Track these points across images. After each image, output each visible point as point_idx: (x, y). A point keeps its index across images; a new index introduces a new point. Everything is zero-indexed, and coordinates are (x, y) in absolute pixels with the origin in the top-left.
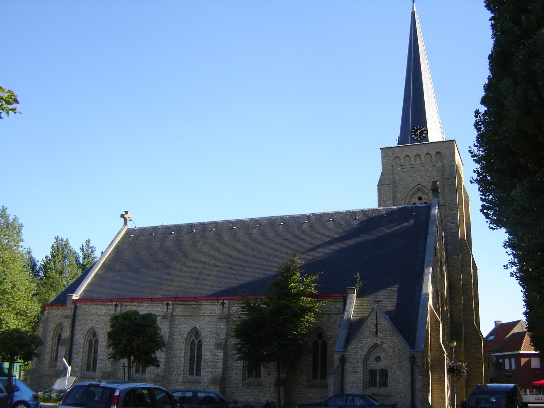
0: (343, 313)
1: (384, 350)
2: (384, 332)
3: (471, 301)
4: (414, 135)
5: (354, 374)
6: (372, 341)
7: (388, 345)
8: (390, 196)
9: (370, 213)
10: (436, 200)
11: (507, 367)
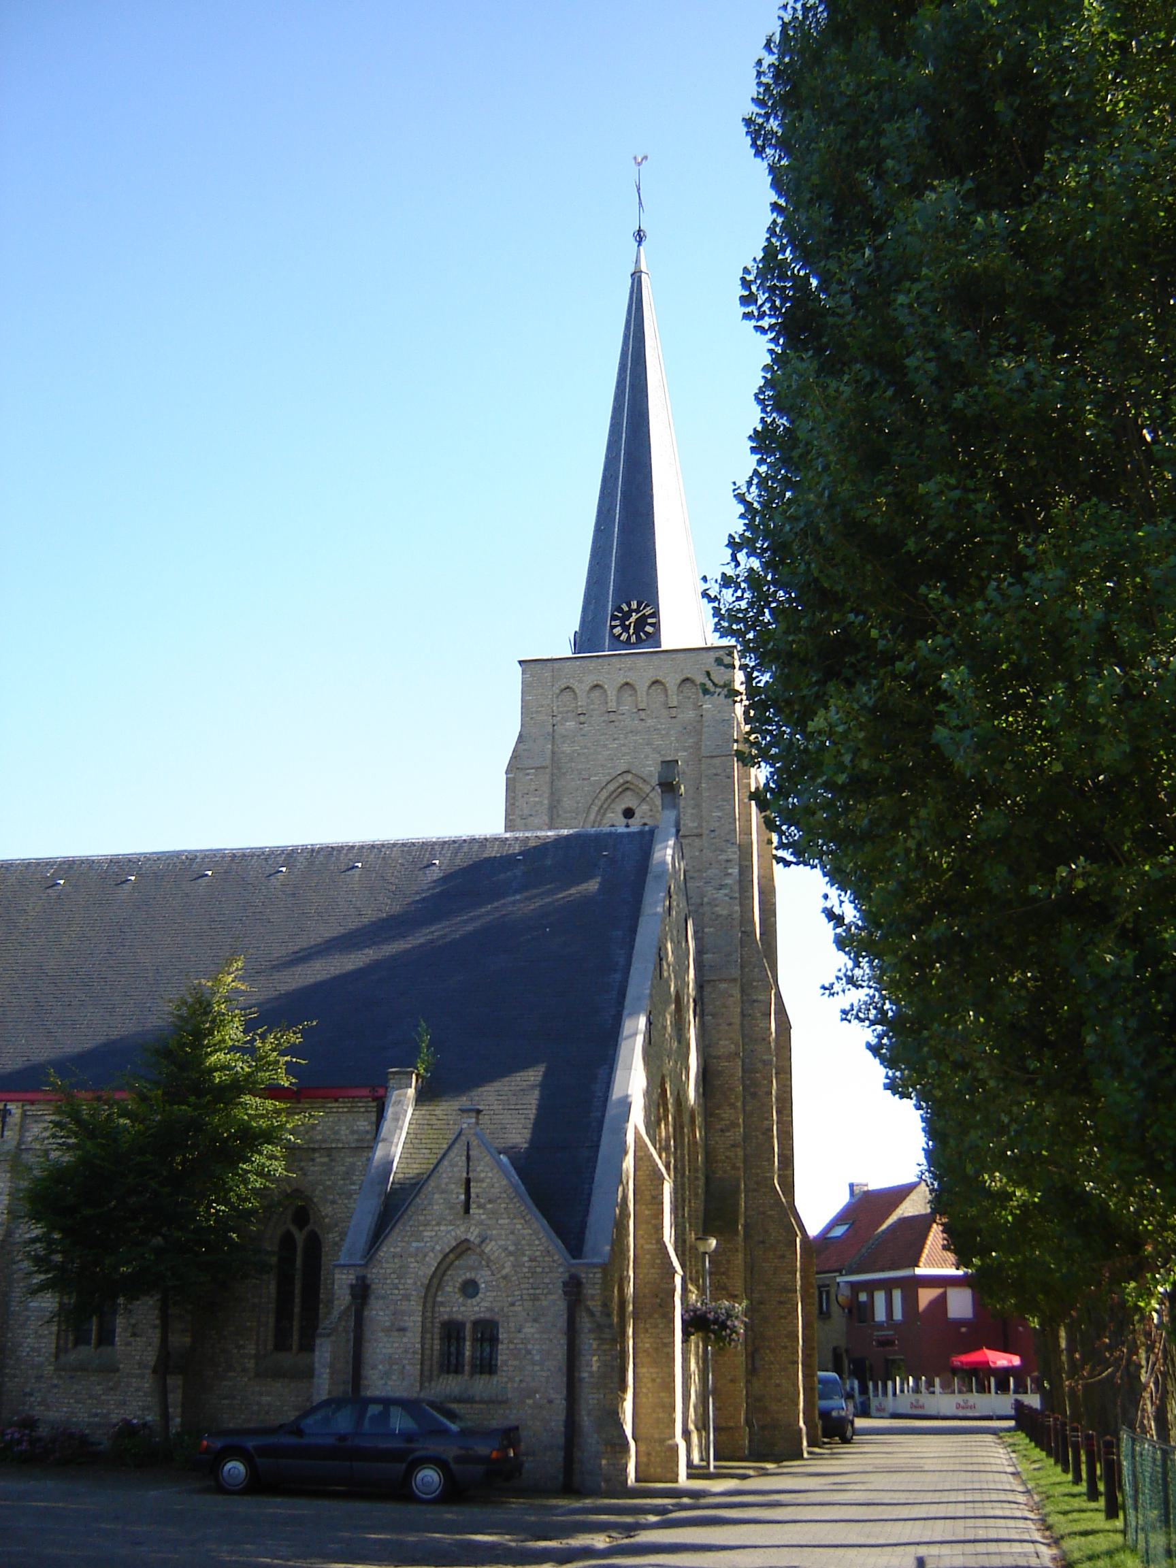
0: (371, 1149)
1: (489, 1260)
2: (489, 1206)
3: (767, 1119)
4: (619, 628)
5: (396, 1333)
6: (453, 1233)
7: (500, 1246)
8: (541, 803)
9: (476, 847)
10: (671, 815)
11: (880, 1315)
